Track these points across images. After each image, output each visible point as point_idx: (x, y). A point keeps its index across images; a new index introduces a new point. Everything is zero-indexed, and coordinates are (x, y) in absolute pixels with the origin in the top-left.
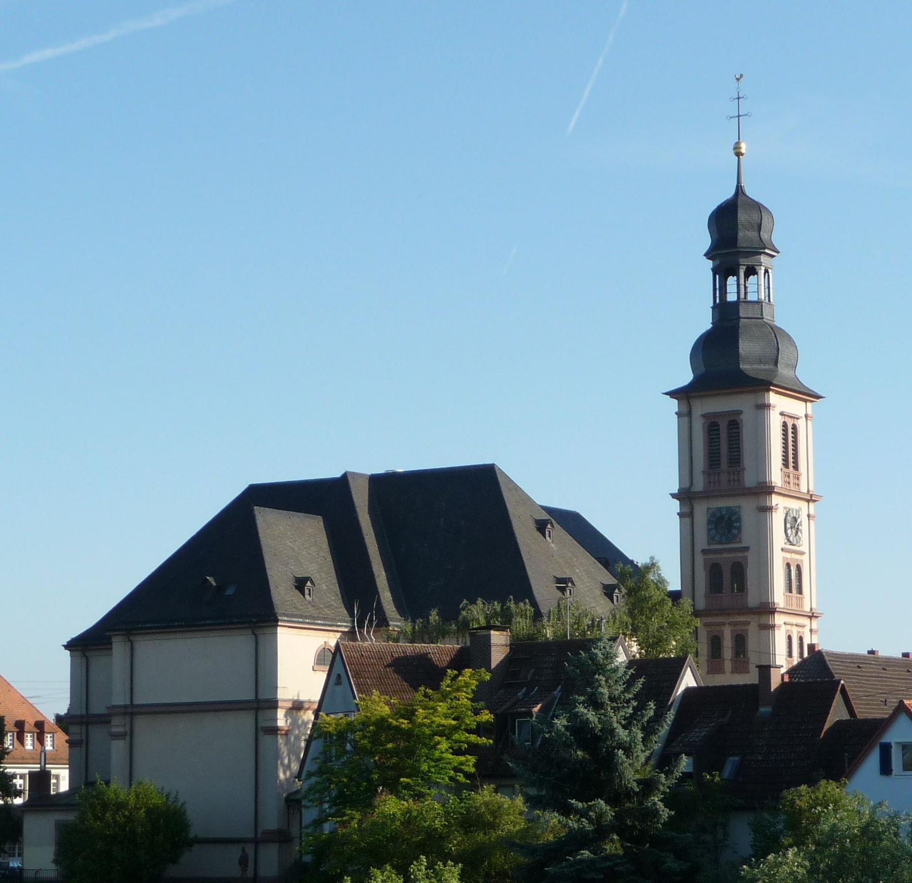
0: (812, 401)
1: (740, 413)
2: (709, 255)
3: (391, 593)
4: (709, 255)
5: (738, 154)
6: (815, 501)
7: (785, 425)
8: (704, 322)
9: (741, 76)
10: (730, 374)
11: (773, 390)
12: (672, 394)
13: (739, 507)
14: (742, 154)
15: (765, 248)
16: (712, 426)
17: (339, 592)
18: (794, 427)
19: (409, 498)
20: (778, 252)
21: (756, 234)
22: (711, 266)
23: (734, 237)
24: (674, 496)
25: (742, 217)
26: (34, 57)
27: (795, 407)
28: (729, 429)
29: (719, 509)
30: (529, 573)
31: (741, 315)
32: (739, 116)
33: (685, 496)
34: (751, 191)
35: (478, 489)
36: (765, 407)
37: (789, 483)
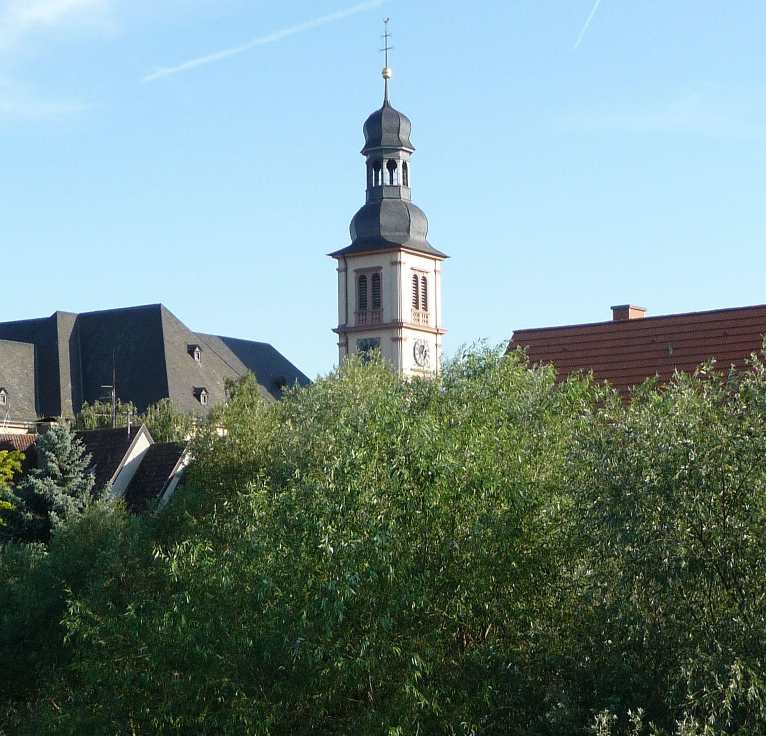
0: (441, 260)
1: (380, 268)
2: (364, 152)
3: (73, 400)
4: (364, 152)
5: (386, 77)
6: (441, 334)
7: (415, 277)
8: (360, 200)
9: (388, 19)
10: (375, 238)
11: (404, 251)
12: (333, 255)
13: (380, 338)
14: (389, 78)
15: (402, 146)
16: (361, 280)
17: (33, 400)
18: (424, 279)
19: (94, 327)
20: (414, 150)
21: (396, 136)
22: (366, 160)
23: (382, 140)
24: (334, 331)
25: (385, 123)
26: (189, 64)
27: (425, 264)
28: (373, 281)
29: (365, 340)
30: (170, 384)
31: (384, 196)
32: (386, 49)
33: (342, 331)
34: (395, 105)
35: (146, 323)
36: (396, 263)
37: (418, 320)
